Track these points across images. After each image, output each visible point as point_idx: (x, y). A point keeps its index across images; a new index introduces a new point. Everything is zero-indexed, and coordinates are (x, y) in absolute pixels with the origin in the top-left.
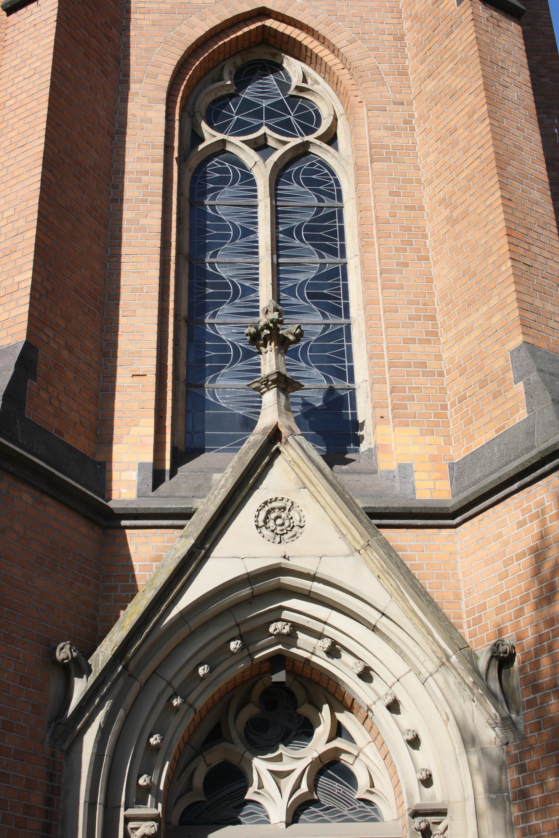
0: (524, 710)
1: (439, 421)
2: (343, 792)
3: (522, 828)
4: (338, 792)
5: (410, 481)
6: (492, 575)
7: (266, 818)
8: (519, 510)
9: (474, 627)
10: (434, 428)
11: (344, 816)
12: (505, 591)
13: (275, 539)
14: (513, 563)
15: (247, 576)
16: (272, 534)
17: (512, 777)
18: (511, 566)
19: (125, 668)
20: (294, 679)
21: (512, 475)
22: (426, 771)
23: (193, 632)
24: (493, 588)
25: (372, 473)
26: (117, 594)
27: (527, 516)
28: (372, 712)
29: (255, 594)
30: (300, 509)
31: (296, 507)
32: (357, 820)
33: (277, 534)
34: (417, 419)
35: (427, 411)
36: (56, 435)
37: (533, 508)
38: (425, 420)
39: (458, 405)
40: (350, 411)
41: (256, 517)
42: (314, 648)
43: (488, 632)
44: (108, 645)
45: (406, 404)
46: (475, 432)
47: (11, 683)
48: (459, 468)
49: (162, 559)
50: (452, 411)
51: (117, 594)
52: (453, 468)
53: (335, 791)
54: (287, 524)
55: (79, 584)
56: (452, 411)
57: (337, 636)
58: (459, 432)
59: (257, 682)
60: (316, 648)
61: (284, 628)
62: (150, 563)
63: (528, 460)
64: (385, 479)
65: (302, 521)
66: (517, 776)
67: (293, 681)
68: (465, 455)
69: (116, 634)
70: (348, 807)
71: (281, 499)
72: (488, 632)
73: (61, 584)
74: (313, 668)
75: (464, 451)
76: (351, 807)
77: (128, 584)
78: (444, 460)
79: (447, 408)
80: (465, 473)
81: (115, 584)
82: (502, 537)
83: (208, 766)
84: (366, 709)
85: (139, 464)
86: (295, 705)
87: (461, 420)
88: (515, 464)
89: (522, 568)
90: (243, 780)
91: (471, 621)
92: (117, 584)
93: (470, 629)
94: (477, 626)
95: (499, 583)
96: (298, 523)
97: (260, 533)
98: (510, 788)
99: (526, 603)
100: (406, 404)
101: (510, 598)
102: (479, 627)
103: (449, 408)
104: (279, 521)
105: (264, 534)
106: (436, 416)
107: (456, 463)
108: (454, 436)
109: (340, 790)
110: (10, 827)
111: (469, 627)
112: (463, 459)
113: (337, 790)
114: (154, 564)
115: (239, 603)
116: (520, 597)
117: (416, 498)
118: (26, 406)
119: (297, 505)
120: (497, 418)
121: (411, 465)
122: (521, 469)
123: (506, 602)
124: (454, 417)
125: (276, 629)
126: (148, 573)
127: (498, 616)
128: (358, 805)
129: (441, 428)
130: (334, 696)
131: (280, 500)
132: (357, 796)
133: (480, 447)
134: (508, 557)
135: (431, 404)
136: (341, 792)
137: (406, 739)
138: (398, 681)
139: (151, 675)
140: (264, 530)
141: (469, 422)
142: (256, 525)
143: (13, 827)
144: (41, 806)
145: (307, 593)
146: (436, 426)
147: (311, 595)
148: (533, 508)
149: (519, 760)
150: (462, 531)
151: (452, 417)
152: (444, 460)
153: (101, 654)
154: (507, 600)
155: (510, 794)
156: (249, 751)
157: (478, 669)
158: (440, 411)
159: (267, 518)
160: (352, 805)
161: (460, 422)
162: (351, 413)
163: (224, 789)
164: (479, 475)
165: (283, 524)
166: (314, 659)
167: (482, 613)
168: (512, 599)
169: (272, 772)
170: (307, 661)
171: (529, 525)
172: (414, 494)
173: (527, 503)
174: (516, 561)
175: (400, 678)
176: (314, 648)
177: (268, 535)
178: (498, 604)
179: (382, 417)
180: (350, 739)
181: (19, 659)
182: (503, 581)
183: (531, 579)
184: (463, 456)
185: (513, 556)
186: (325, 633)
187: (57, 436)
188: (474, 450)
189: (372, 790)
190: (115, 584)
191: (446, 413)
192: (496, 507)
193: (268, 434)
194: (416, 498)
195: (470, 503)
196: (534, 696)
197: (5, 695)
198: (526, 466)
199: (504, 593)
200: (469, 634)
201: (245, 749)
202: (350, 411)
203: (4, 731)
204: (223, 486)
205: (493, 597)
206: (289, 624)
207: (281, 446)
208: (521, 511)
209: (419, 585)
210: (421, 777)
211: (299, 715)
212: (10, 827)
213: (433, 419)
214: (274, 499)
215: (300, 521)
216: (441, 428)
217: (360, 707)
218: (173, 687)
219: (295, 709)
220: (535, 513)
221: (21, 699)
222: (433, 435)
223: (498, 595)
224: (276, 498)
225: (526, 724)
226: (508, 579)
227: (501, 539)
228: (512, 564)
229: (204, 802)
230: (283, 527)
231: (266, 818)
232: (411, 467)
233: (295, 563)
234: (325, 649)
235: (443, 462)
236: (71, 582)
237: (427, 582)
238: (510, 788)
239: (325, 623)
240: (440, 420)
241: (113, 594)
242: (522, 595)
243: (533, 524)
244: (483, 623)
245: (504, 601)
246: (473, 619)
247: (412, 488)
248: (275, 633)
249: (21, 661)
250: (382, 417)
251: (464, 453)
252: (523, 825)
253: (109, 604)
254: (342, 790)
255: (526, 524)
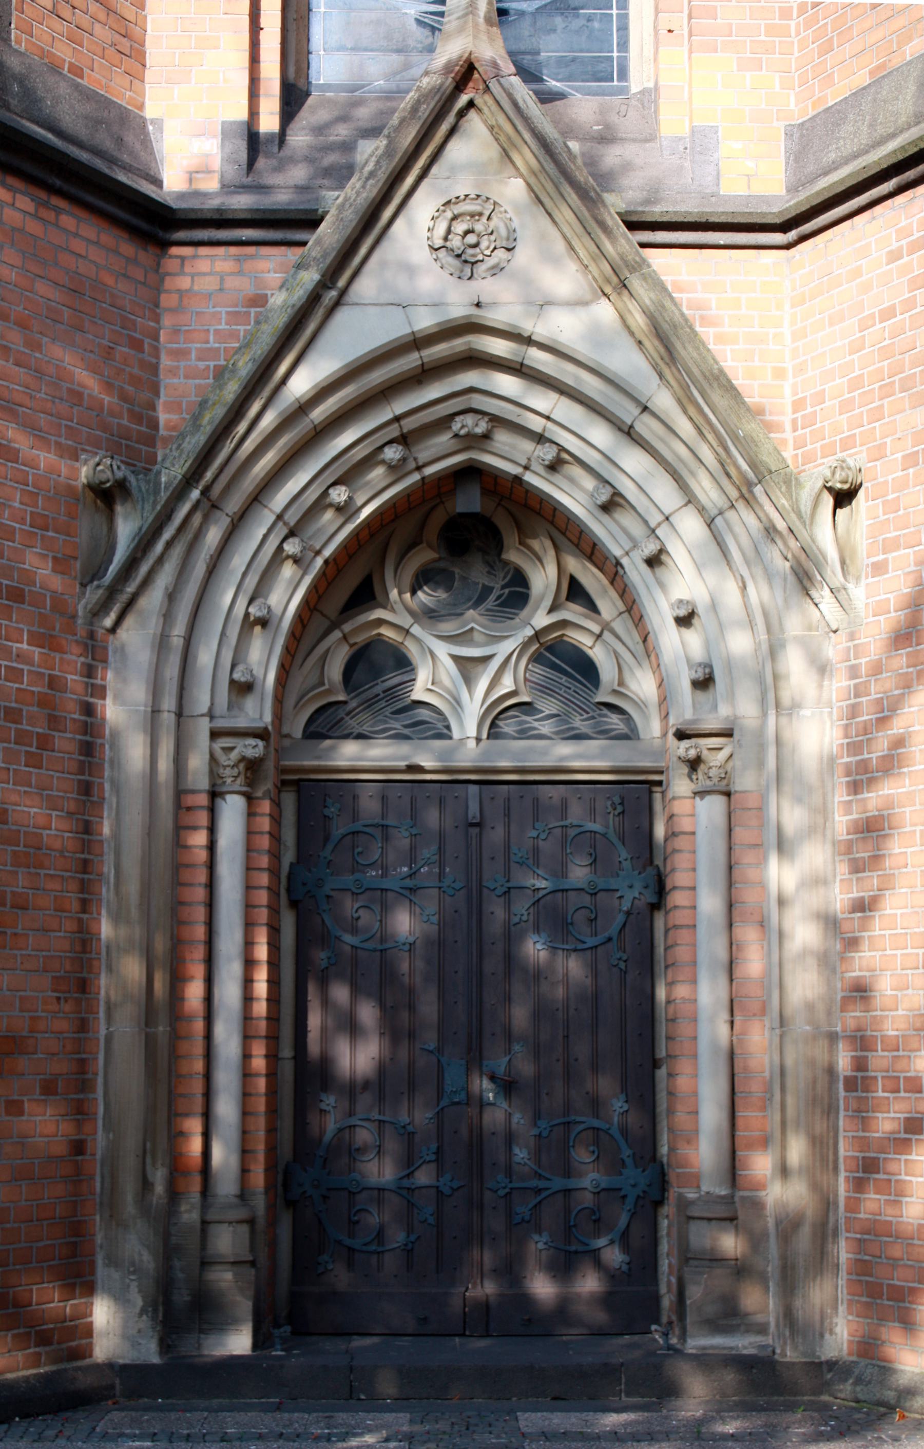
0: (867, 578)
1: (775, 41)
2: (575, 691)
3: (847, 763)
4: (565, 692)
5: (712, 160)
6: (839, 343)
7: (445, 731)
8: (893, 230)
9: (804, 431)
10: (764, 56)
11: (573, 729)
12: (857, 373)
13: (462, 271)
14: (874, 325)
15: (412, 338)
16: (456, 263)
17: (839, 684)
18: (871, 330)
19: (205, 492)
20: (499, 504)
21: (885, 166)
22: (705, 667)
23: (321, 431)
24: (839, 365)
25: (647, 141)
26: (189, 363)
27: (904, 242)
28: (623, 567)
29: (426, 367)
30: (508, 216)
31: (501, 213)
32: (595, 735)
33: (466, 262)
34: (734, 38)
35: (752, 22)
36: (69, 75)
37: (915, 228)
38: (748, 39)
39: (810, 12)
40: (614, 12)
41: (429, 230)
42: (529, 459)
43: (824, 442)
44: (175, 458)
45: (715, 8)
46: (836, 69)
47: (17, 526)
48: (802, 136)
49: (263, 306)
50: (799, 22)
51: (189, 363)
52: (792, 135)
53: (561, 689)
54: (484, 244)
55: (123, 349)
56: (799, 22)
57: (567, 440)
58: (809, 67)
59: (433, 508)
60: (532, 459)
61: (477, 425)
62: (245, 310)
63: (914, 141)
64: (668, 153)
65: (512, 239)
66: (848, 683)
67: (496, 507)
68: (815, 113)
69: (187, 439)
70: (582, 715)
71: (474, 196)
72: (824, 442)
73: (91, 351)
74: (527, 491)
75: (814, 104)
76: (586, 716)
77: (208, 346)
78: (778, 120)
79: (792, 15)
80: (812, 147)
81: (185, 346)
82: (861, 276)
83: (351, 646)
84: (614, 562)
85: (223, 123)
86: (499, 547)
87: (813, 43)
88: (892, 146)
89: (887, 336)
90: (408, 669)
91: (799, 420)
92: (190, 345)
93: (797, 434)
94: (808, 430)
95: (848, 358)
96: (504, 244)
97: (436, 260)
98: (834, 700)
99: (887, 397)
100: (715, 8)
101: (864, 387)
102: (810, 432)
103: (795, 16)
104: (471, 239)
105: (444, 261)
106: (771, 30)
107: (799, 125)
108: (799, 72)
109: (569, 688)
110: (28, 749)
111: (795, 430)
112: (810, 119)
113: (564, 689)
114: (253, 310)
115: (400, 383)
116: (881, 387)
117: (721, 193)
118: (13, 26)
119: (502, 209)
120: (874, 47)
121: (715, 130)
122: (900, 157)
123: (856, 393)
124: (803, 34)
125: (463, 427)
126: (242, 328)
127: (842, 416)
128: (598, 712)
129: (777, 56)
130: (564, 534)
131: (473, 199)
132: (597, 700)
133: (841, 101)
134: (867, 313)
135: (762, 7)
136: (571, 692)
137: (675, 615)
138: (667, 519)
139: (251, 504)
140: (442, 254)
141: (827, 49)
142: (429, 245)
143: (33, 749)
144: (76, 716)
145: (518, 367)
146: (767, 52)
147: (524, 370)
148: (915, 228)
149: (852, 658)
150: (798, 257)
151: (798, 34)
152: (778, 120)
153: (163, 470)
154: (859, 389)
155: (835, 709)
156: (420, 625)
157: (798, 507)
158: (777, 21)
159: (449, 231)
160: (588, 713)
161: (812, 46)
162: (617, 14)
163: (377, 684)
164: (833, 156)
165: (476, 245)
166: (529, 477)
167: (818, 408)
168: (867, 389)
169: (456, 659)
170: (518, 479)
171: (906, 259)
172: (718, 185)
173: (907, 218)
174: (881, 322)
175: (670, 515)
176: (529, 459)
177: (450, 265)
178: (843, 395)
179: (670, 31)
180: (592, 606)
181: (28, 485)
182: (855, 356)
183: (61, 1138)
184: (811, 113)
185: (874, 313)
186: (546, 435)
187: (72, 77)
188: (830, 104)
189: (622, 690)
190: (185, 346)
191: (789, 26)
192: (856, 219)
193: (453, 75)
194: (721, 193)
195: (812, 208)
196: (885, 556)
197: (8, 546)
198: (910, 153)
199: (856, 377)
200: (795, 442)
201: (412, 621)
202: (614, 12)
203: (11, 603)
204: (372, 174)
205: (838, 381)
206: (486, 419)
207: (477, 96)
208: (896, 231)
209: (710, 358)
210: (694, 676)
211: (506, 563)
212: (28, 749)
213: (763, 38)
214: (462, 197)
215: (508, 239)
216: (777, 56)
217: (607, 558)
218: (285, 524)
219: (499, 554)
220: (918, 238)
221: (34, 550)
222: (761, 69)
223: (845, 379)
224: (467, 196)
225: (870, 601)
226: (864, 352)
227: (859, 280)
228: (873, 326)
229: (345, 703)
230: (477, 250)
231: (445, 731)
232: (716, 132)
233: (497, 317)
234: (547, 463)
235: (775, 124)
236: (110, 347)
237: (728, 348)
238: (834, 700)
239: (548, 418)
240: (777, 39)
241: (182, 364)
242: (883, 383)
243: (913, 259)
244: (818, 425)
245: (854, 391)
246: (803, 416)
247: (715, 173)
248: (462, 432)
249: (30, 488)
250: (670, 31)
251: (813, 109)
252: (848, 760)
253: (176, 381)
254: (573, 688)
255: (900, 257)
